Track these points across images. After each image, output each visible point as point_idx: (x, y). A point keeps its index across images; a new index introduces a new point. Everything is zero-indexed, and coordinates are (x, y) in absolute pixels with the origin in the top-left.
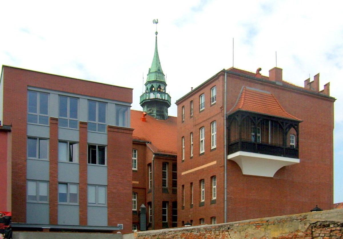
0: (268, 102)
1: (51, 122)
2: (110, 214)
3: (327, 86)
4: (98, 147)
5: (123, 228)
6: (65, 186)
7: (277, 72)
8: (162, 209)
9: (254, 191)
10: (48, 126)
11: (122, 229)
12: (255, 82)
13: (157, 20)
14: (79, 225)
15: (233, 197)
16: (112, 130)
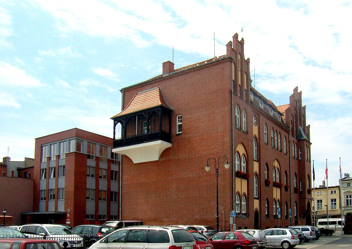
7: (168, 66)
9: (143, 176)
16: (67, 155)
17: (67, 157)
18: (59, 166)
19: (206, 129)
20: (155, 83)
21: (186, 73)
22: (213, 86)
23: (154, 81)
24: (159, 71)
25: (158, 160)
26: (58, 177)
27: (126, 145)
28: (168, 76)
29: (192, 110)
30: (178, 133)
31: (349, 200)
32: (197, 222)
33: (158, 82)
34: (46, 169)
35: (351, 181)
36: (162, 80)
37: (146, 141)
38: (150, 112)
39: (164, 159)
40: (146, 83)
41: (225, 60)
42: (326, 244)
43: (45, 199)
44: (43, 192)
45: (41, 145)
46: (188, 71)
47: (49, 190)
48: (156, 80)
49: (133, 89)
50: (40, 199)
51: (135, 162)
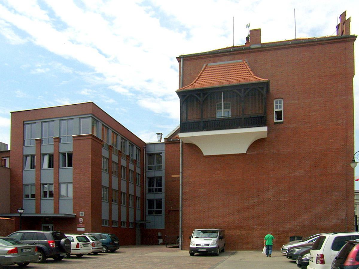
0: (224, 71)
1: (74, 139)
2: (74, 204)
3: (349, 19)
4: (67, 154)
5: (83, 215)
6: (60, 184)
7: (255, 34)
8: (30, 198)
9: (219, 172)
10: (34, 146)
11: (83, 215)
12: (210, 56)
13: (249, 24)
14: (53, 213)
15: (191, 181)
16: (76, 139)
17: (74, 141)
18: (59, 153)
19: (321, 119)
20: (238, 54)
21: (289, 48)
22: (330, 68)
23: (235, 51)
24: (240, 41)
25: (246, 154)
26: (23, 169)
27: (239, 127)
28: (259, 48)
29: (298, 94)
30: (275, 121)
31: (157, 210)
32: (306, 229)
33: (243, 53)
34: (33, 156)
35: (358, 193)
36: (250, 52)
37: (241, 126)
38: (248, 89)
39: (255, 153)
40: (216, 53)
41: (350, 39)
42: (195, 237)
43: (33, 196)
44: (30, 188)
45: (24, 122)
46: (292, 46)
47: (41, 184)
48: (241, 50)
49: (200, 58)
50: (24, 196)
51: (205, 154)
